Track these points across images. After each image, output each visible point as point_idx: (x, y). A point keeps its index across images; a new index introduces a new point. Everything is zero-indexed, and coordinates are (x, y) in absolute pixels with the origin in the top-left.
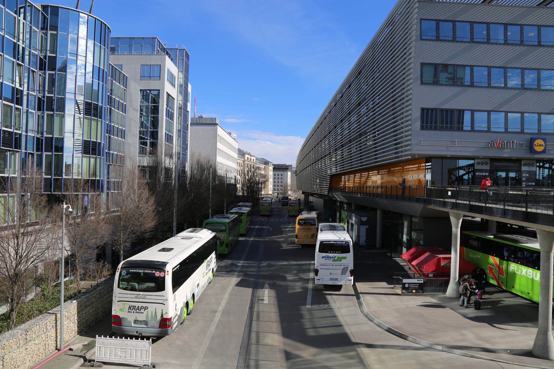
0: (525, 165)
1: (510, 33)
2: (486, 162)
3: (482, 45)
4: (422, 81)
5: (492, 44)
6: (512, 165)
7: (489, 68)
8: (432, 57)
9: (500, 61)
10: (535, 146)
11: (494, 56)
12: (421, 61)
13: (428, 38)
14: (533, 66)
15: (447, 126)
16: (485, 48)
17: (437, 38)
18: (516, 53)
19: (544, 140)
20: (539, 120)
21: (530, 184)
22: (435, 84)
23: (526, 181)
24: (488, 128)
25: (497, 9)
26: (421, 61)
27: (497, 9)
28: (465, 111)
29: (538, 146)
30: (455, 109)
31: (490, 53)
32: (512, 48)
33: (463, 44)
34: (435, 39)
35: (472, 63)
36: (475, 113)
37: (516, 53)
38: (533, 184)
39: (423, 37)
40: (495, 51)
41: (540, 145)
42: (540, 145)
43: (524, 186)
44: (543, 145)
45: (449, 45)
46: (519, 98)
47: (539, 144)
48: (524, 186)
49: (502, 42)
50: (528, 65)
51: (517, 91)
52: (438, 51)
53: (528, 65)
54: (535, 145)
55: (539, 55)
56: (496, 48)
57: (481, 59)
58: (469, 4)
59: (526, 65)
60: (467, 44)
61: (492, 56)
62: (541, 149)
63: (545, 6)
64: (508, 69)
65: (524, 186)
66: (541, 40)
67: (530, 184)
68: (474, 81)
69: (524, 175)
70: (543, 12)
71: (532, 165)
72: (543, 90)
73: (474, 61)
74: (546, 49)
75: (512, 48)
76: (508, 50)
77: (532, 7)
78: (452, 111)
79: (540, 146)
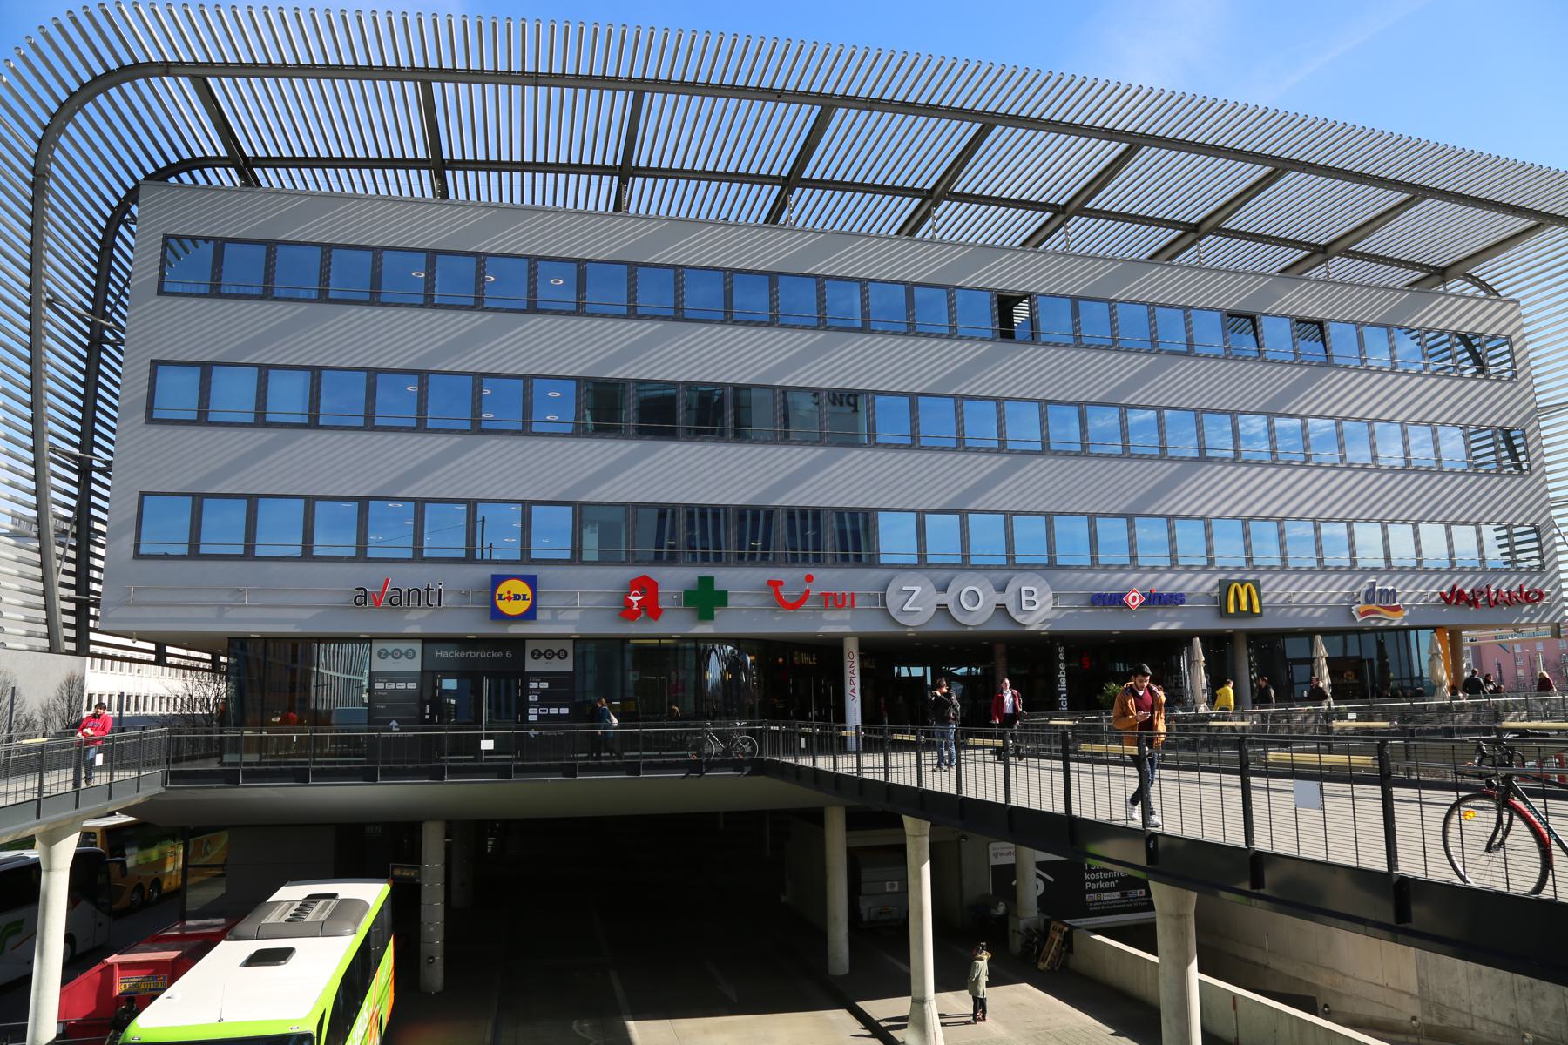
0: (536, 655)
1: (493, 279)
2: (411, 650)
3: (354, 309)
4: (149, 412)
5: (593, 315)
6: (494, 655)
7: (372, 373)
8: (334, 346)
9: (1184, 391)
10: (500, 598)
11: (206, 327)
12: (154, 354)
13: (187, 289)
14: (659, 373)
15: (814, 550)
16: (362, 317)
17: (211, 290)
18: (459, 330)
19: (531, 581)
20: (1351, 534)
21: (554, 711)
22: (818, 442)
23: (540, 704)
24: (246, 547)
25: (408, 211)
26: (154, 354)
27: (408, 211)
28: (479, 504)
29: (509, 598)
30: (825, 509)
31: (338, 329)
32: (617, 327)
33: (293, 306)
34: (574, 309)
35: (317, 359)
36: (479, 504)
37: (459, 330)
38: (565, 711)
39: (167, 288)
40: (929, 353)
41: (517, 597)
42: (517, 597)
43: (535, 718)
44: (524, 596)
45: (771, 336)
46: (463, 459)
47: (514, 592)
48: (535, 718)
49: (858, 324)
50: (1230, 403)
51: (456, 439)
52: (213, 327)
53: (1230, 403)
54: (500, 596)
55: (596, 346)
56: (746, 335)
57: (348, 349)
58: (980, 246)
59: (1063, 393)
60: (305, 307)
61: (749, 352)
62: (519, 607)
63: (1167, 260)
64: (1006, 403)
65: (533, 718)
66: (536, 296)
67: (554, 711)
68: (321, 412)
69: (534, 685)
70: (545, 222)
71: (558, 654)
72: (1098, 456)
73: (373, 357)
74: (903, 343)
75: (617, 327)
76: (913, 355)
77: (1137, 261)
78: (817, 513)
79: (515, 599)
